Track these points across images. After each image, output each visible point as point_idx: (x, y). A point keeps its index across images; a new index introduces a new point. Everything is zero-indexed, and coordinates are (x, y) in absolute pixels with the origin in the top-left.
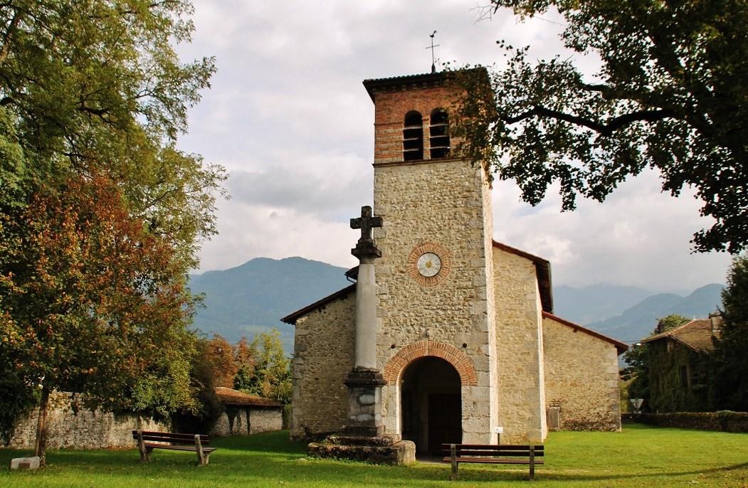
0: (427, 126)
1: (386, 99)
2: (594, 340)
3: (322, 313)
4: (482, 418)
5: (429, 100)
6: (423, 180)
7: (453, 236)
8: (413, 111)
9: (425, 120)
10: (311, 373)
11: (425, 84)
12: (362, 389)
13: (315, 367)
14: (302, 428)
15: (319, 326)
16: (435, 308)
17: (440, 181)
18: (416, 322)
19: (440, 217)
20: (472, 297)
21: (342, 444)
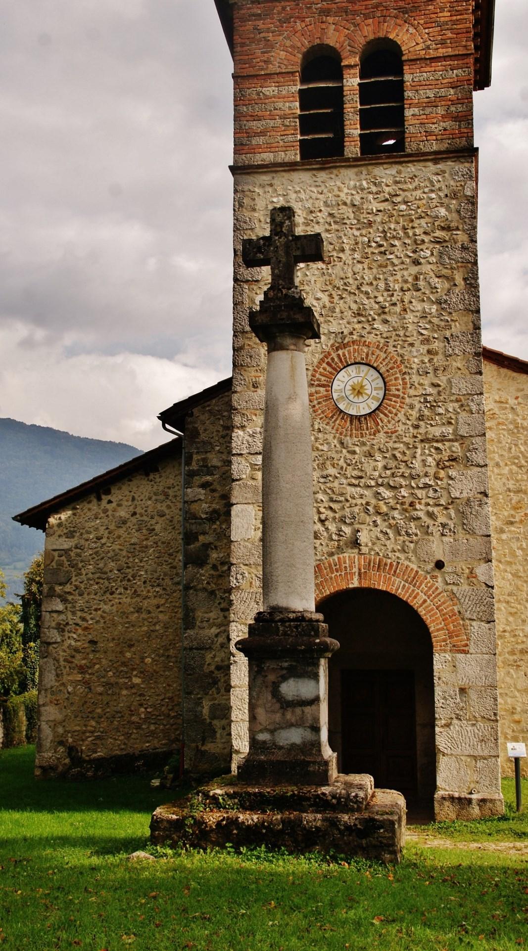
0: (352, 82)
3: (104, 503)
4: (480, 724)
6: (345, 204)
7: (411, 327)
9: (350, 67)
10: (80, 631)
12: (286, 664)
13: (88, 617)
14: (61, 749)
16: (373, 483)
17: (382, 206)
18: (330, 514)
19: (382, 285)
20: (454, 460)
21: (244, 808)
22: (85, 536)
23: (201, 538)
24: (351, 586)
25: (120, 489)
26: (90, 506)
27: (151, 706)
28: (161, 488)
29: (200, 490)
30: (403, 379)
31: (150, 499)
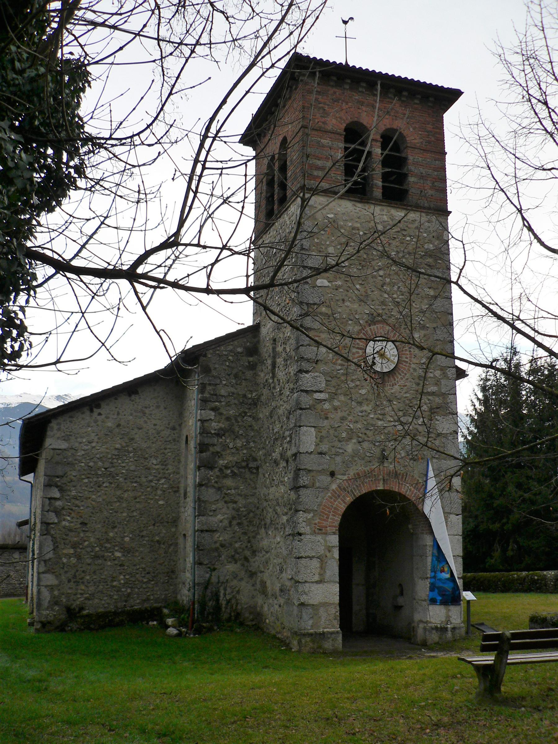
3: (95, 414)
22: (79, 440)
23: (211, 449)
25: (108, 405)
27: (128, 574)
28: (140, 407)
29: (211, 412)
30: (410, 351)
31: (131, 415)
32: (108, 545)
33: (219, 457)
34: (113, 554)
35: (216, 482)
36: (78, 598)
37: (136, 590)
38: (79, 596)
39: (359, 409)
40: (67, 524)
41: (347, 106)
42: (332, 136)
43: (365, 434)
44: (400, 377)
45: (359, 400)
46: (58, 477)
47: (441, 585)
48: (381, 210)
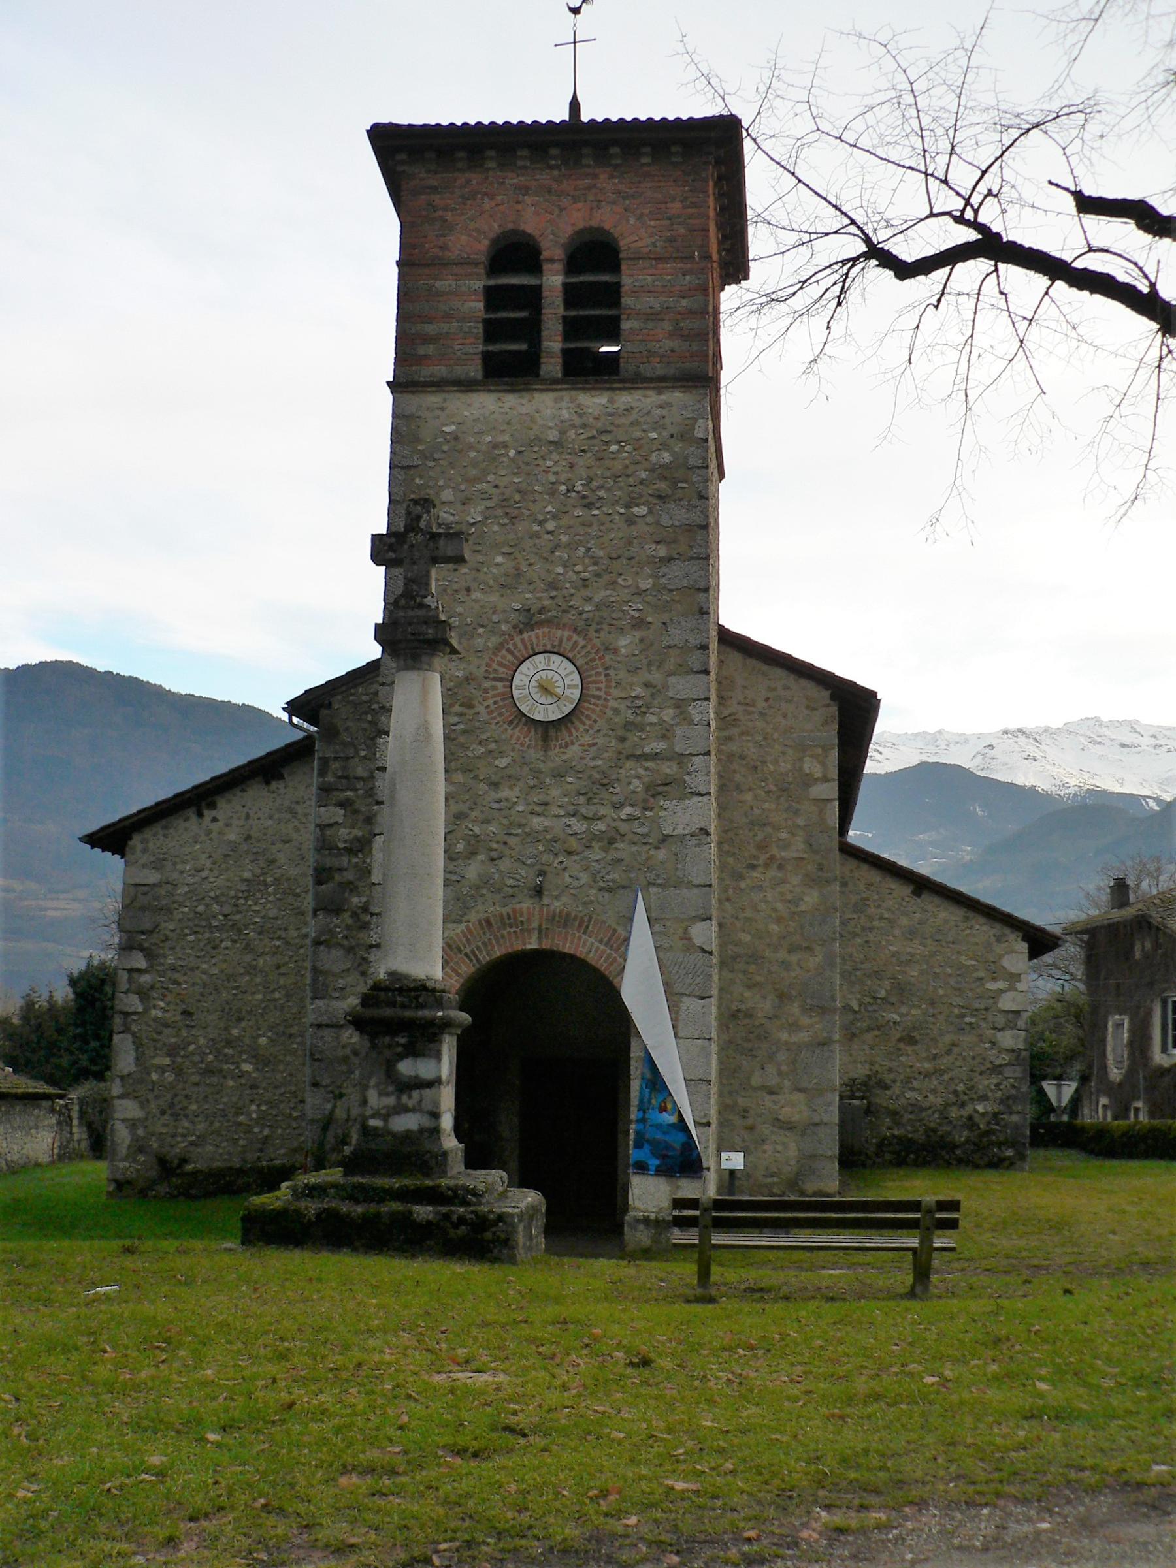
0: (553, 280)
1: (434, 189)
2: (966, 919)
5: (565, 201)
8: (514, 232)
9: (551, 261)
11: (554, 151)
12: (403, 1041)
15: (195, 859)
22: (179, 867)
23: (337, 877)
24: (529, 947)
26: (187, 824)
27: (267, 1103)
30: (607, 675)
31: (271, 817)
32: (230, 1052)
33: (351, 891)
34: (237, 1067)
35: (346, 937)
36: (178, 1143)
37: (280, 1131)
38: (179, 1139)
39: (493, 795)
40: (160, 1014)
41: (493, 204)
42: (456, 269)
43: (505, 843)
44: (582, 728)
45: (494, 778)
46: (143, 933)
47: (659, 1136)
48: (556, 400)
